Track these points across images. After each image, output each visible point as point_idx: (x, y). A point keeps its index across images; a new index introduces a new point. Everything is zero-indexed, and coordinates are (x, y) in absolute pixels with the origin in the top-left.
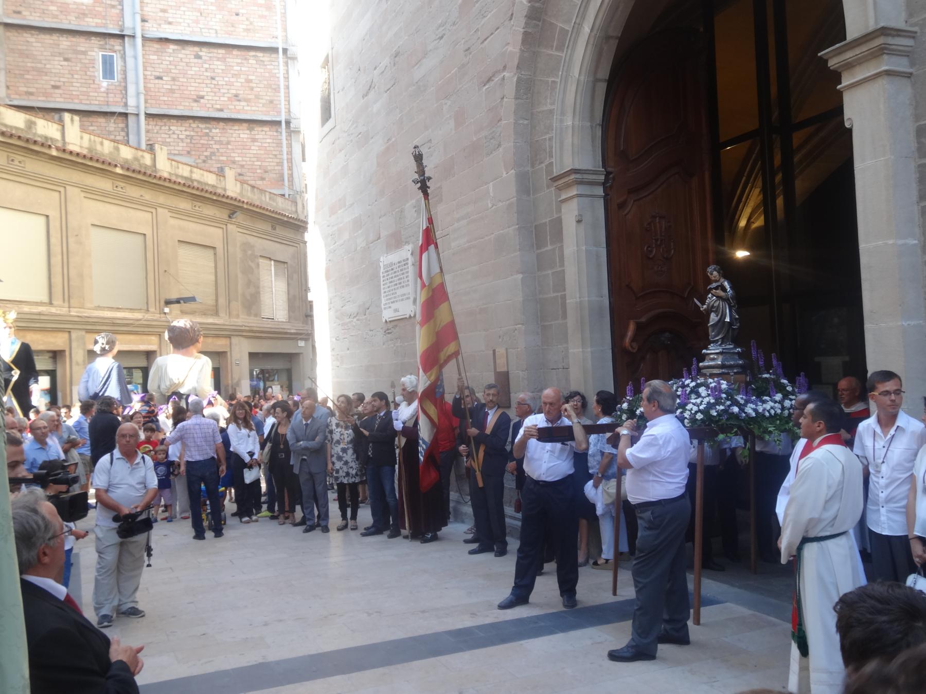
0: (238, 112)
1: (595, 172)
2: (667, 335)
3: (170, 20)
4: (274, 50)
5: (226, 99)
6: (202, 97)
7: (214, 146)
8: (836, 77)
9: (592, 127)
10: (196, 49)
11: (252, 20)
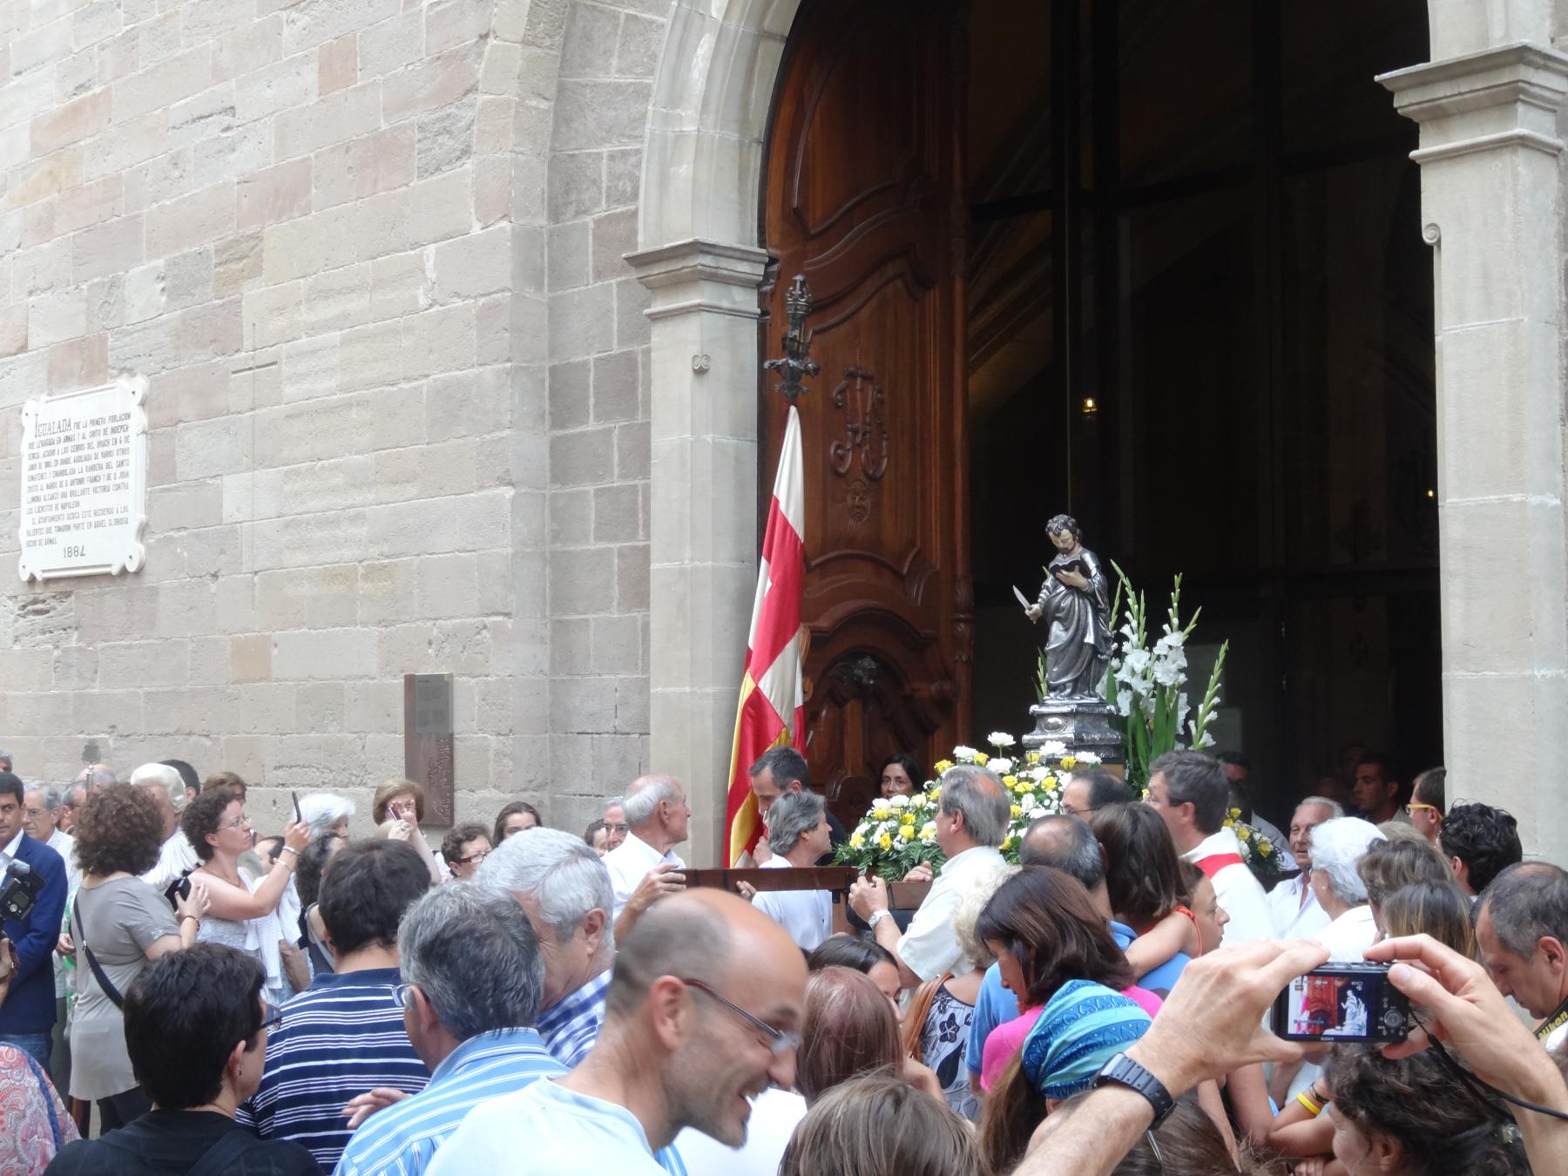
1: (744, 256)
2: (868, 663)
8: (1408, 133)
9: (741, 144)
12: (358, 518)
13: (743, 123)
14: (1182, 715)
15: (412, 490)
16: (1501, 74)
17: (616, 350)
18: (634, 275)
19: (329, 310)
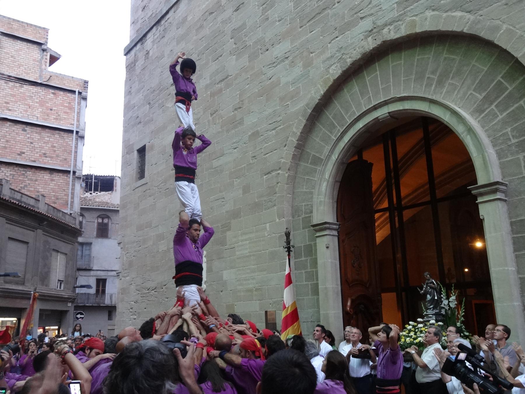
0: (48, 163)
3: (10, 108)
4: (71, 132)
5: (38, 155)
6: (24, 153)
7: (27, 182)
8: (475, 197)
10: (24, 126)
11: (59, 114)
12: (253, 279)
13: (333, 199)
14: (456, 313)
15: (265, 273)
16: (493, 187)
17: (308, 243)
18: (312, 228)
19: (247, 237)
